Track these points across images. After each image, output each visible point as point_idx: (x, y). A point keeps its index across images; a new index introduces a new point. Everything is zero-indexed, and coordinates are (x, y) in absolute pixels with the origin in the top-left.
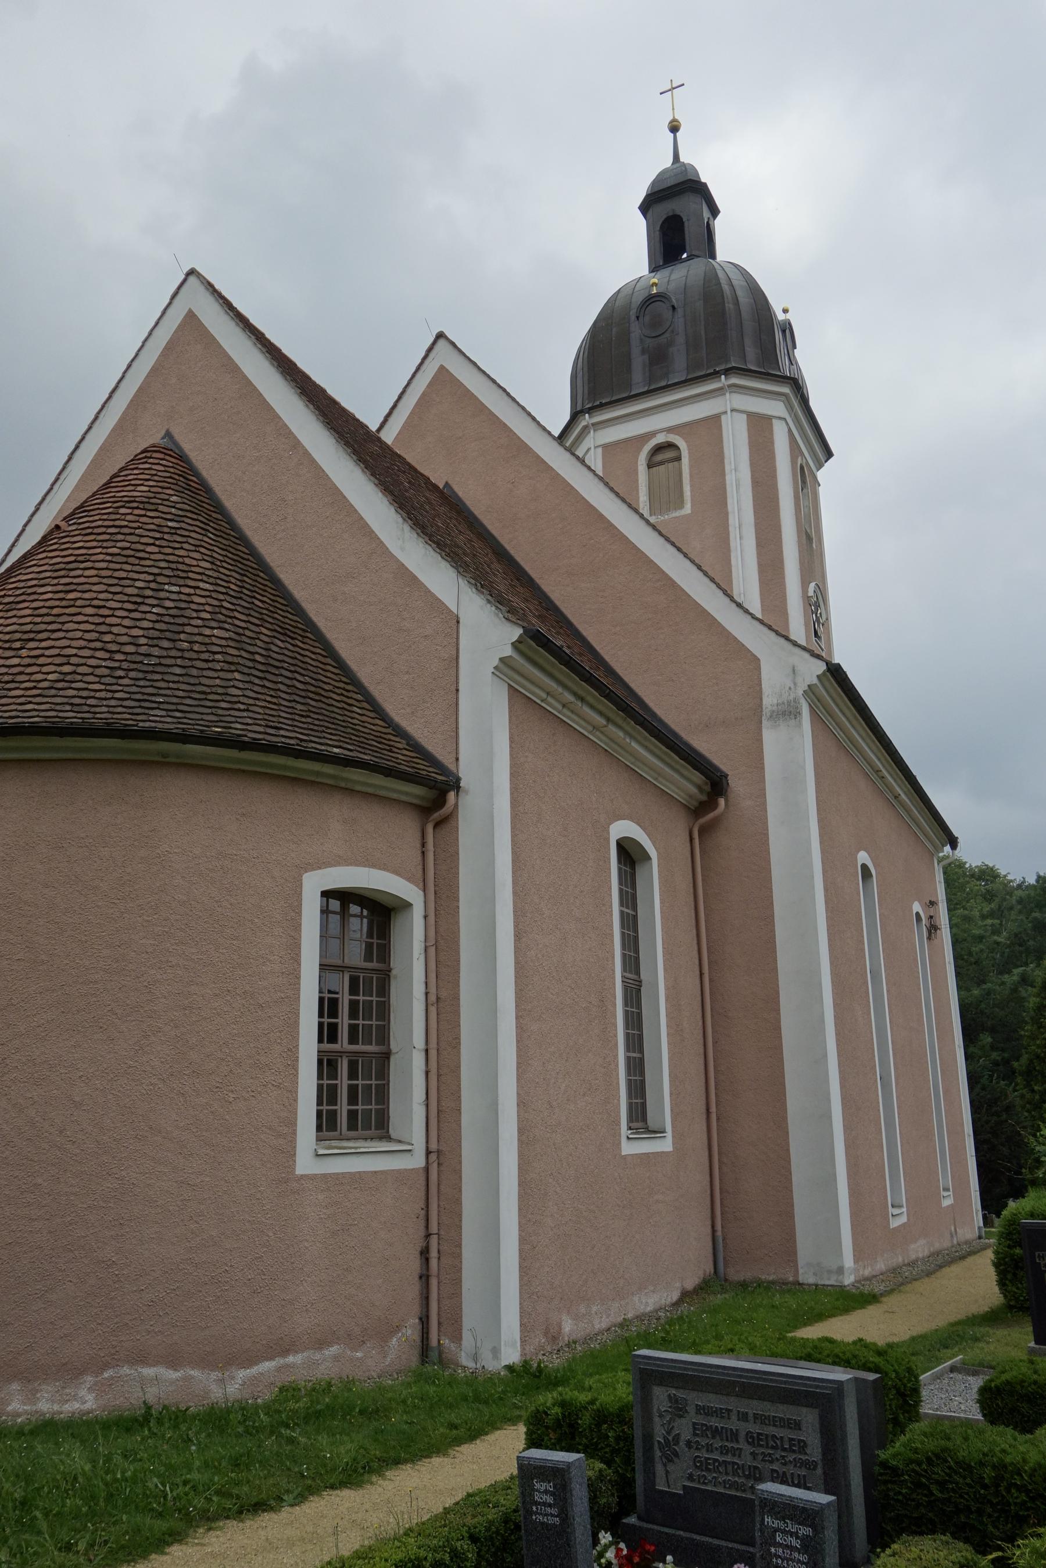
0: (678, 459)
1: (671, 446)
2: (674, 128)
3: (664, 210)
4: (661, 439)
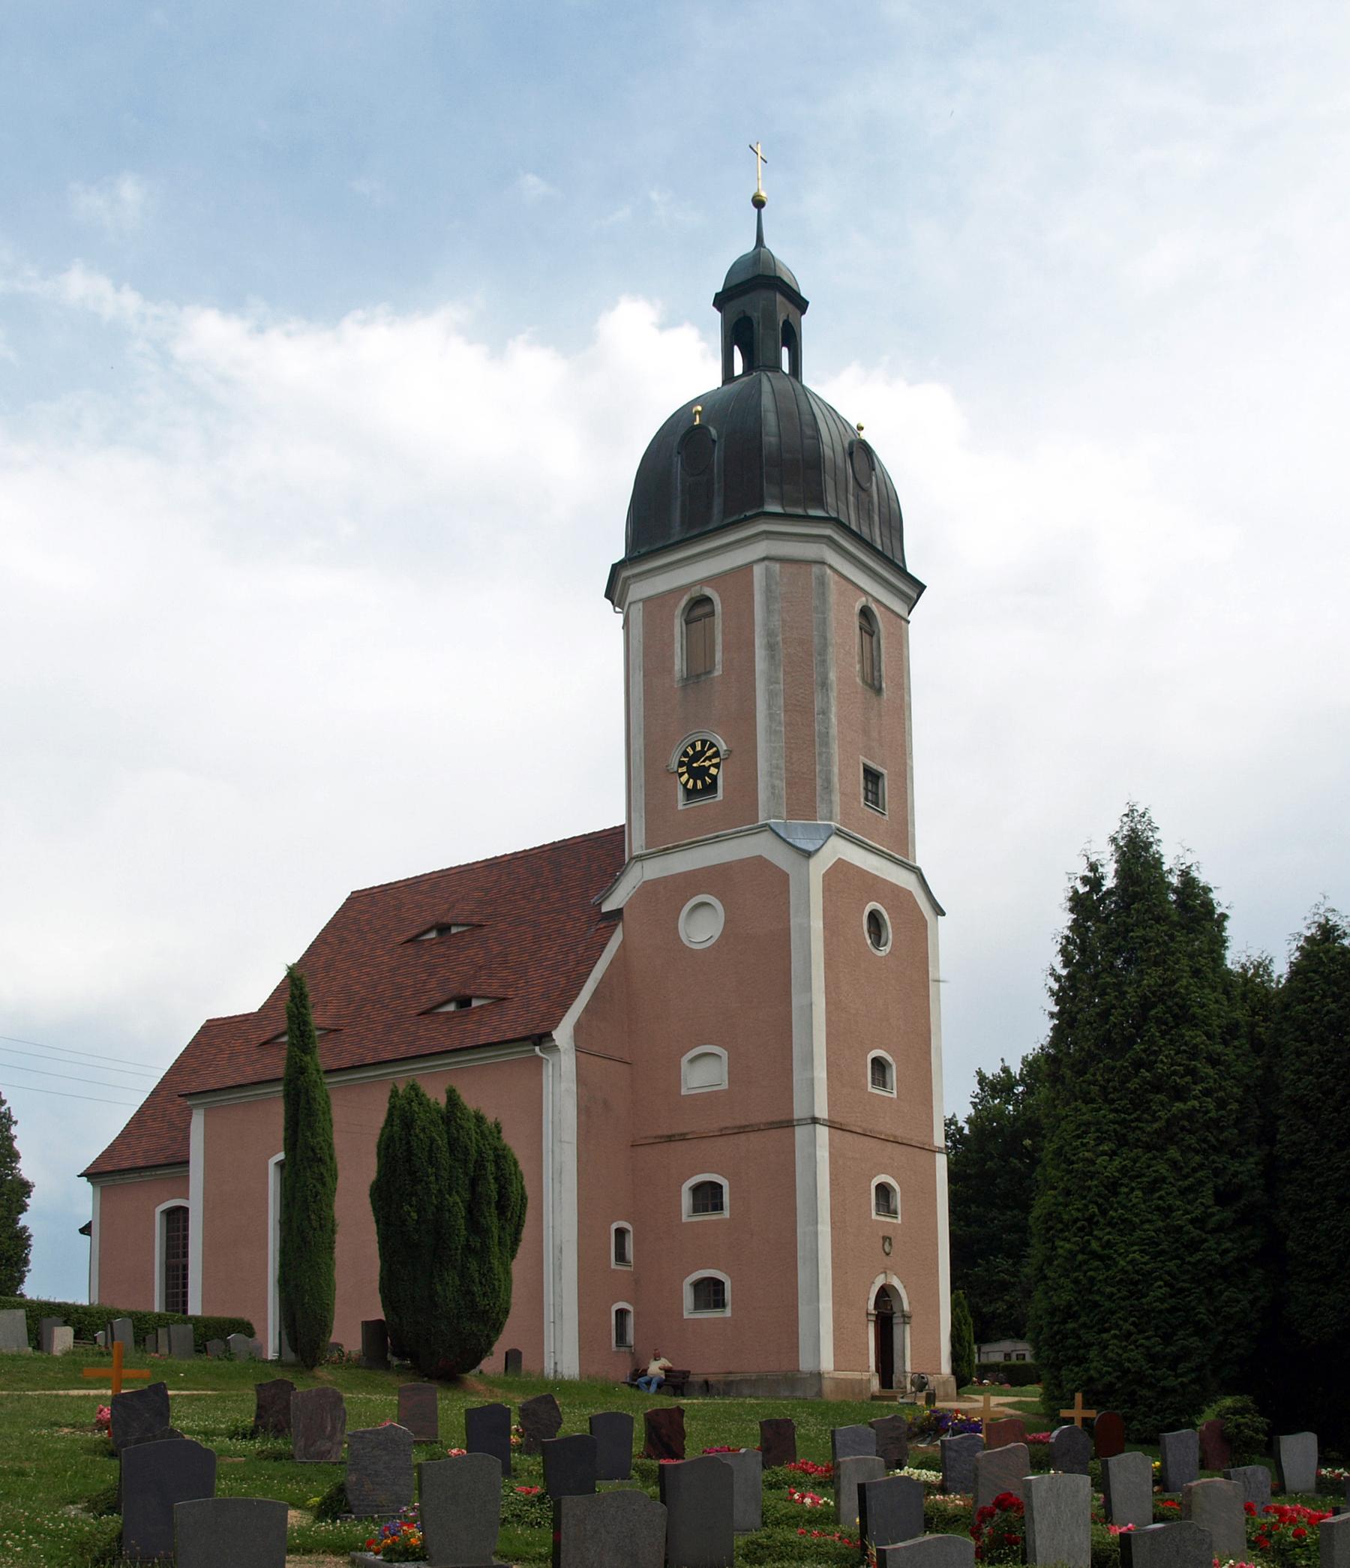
0: (712, 614)
1: (706, 600)
2: (759, 203)
3: (736, 306)
4: (695, 592)
